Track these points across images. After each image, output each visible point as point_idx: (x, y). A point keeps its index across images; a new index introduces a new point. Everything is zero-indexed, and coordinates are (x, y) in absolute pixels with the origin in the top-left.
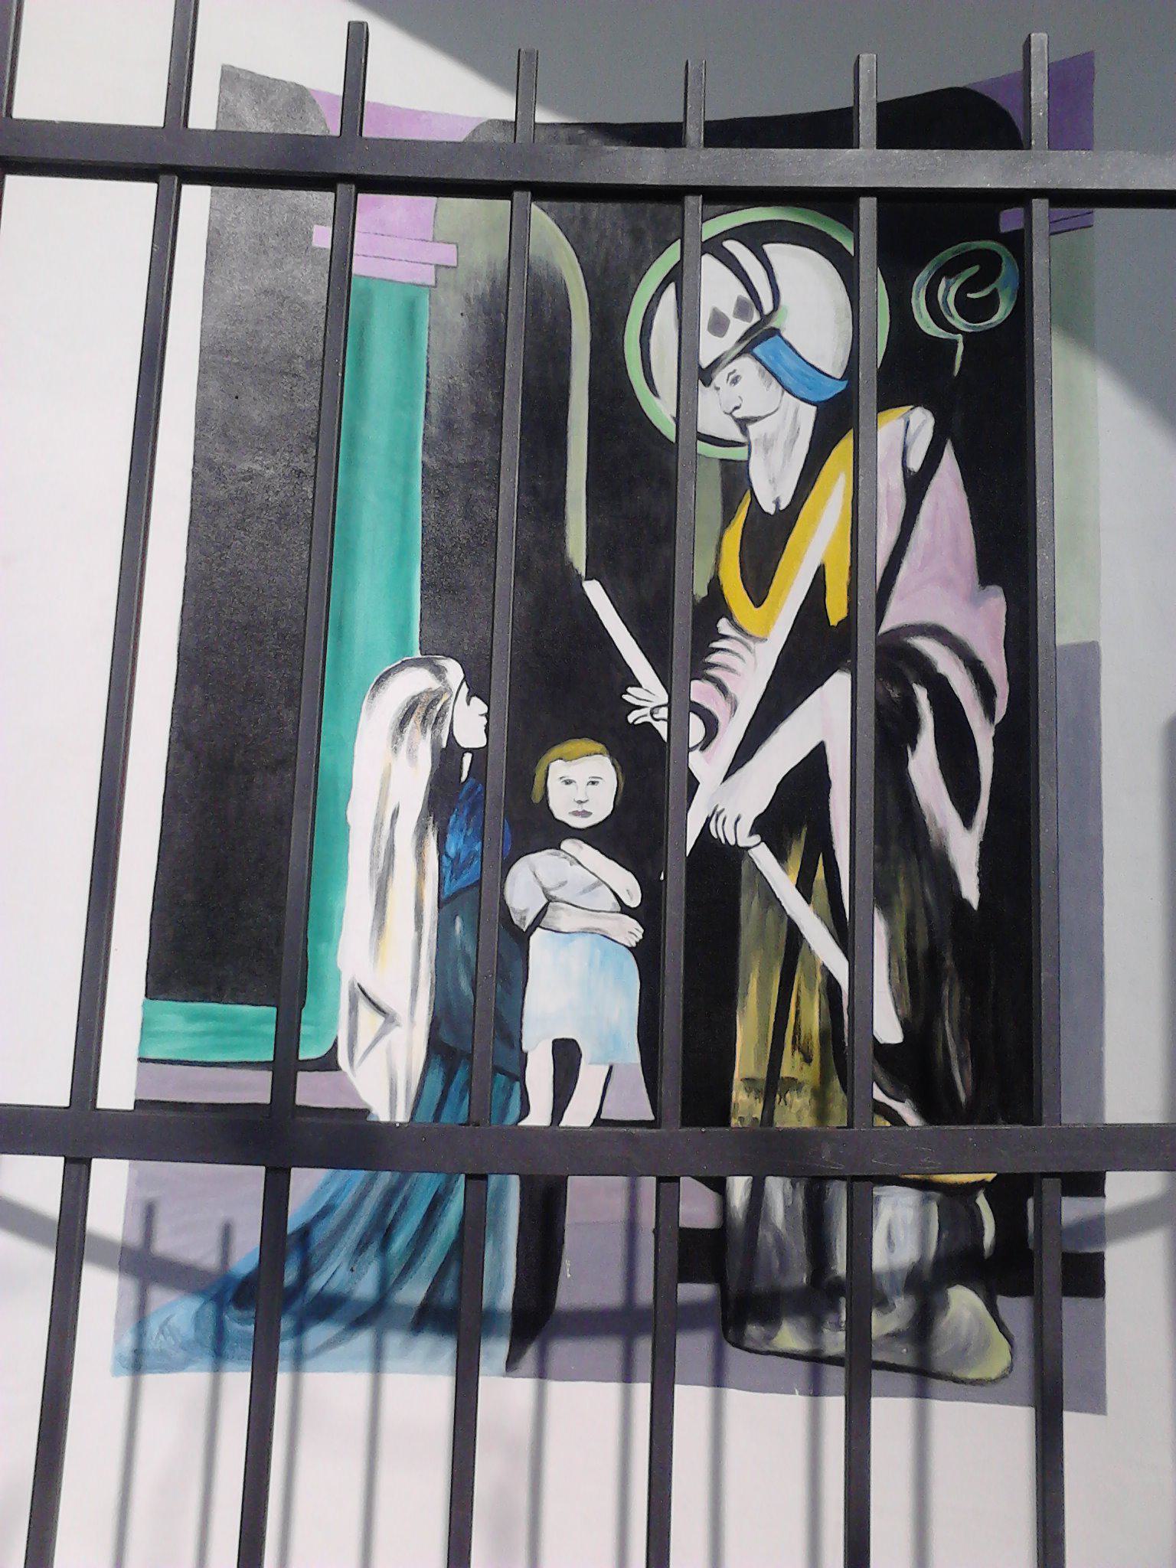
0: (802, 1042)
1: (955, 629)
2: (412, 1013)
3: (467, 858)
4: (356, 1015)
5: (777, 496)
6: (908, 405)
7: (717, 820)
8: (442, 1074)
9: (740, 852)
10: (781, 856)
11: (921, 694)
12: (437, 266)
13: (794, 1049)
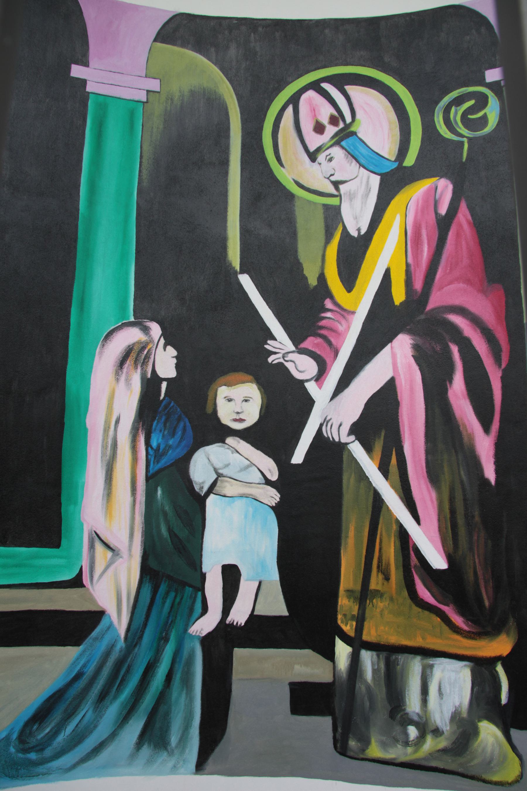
0: (383, 567)
1: (473, 309)
2: (130, 550)
3: (164, 449)
4: (94, 552)
5: (358, 227)
6: (436, 177)
7: (327, 426)
8: (150, 588)
9: (341, 447)
10: (368, 449)
11: (455, 350)
12: (148, 91)
13: (378, 571)
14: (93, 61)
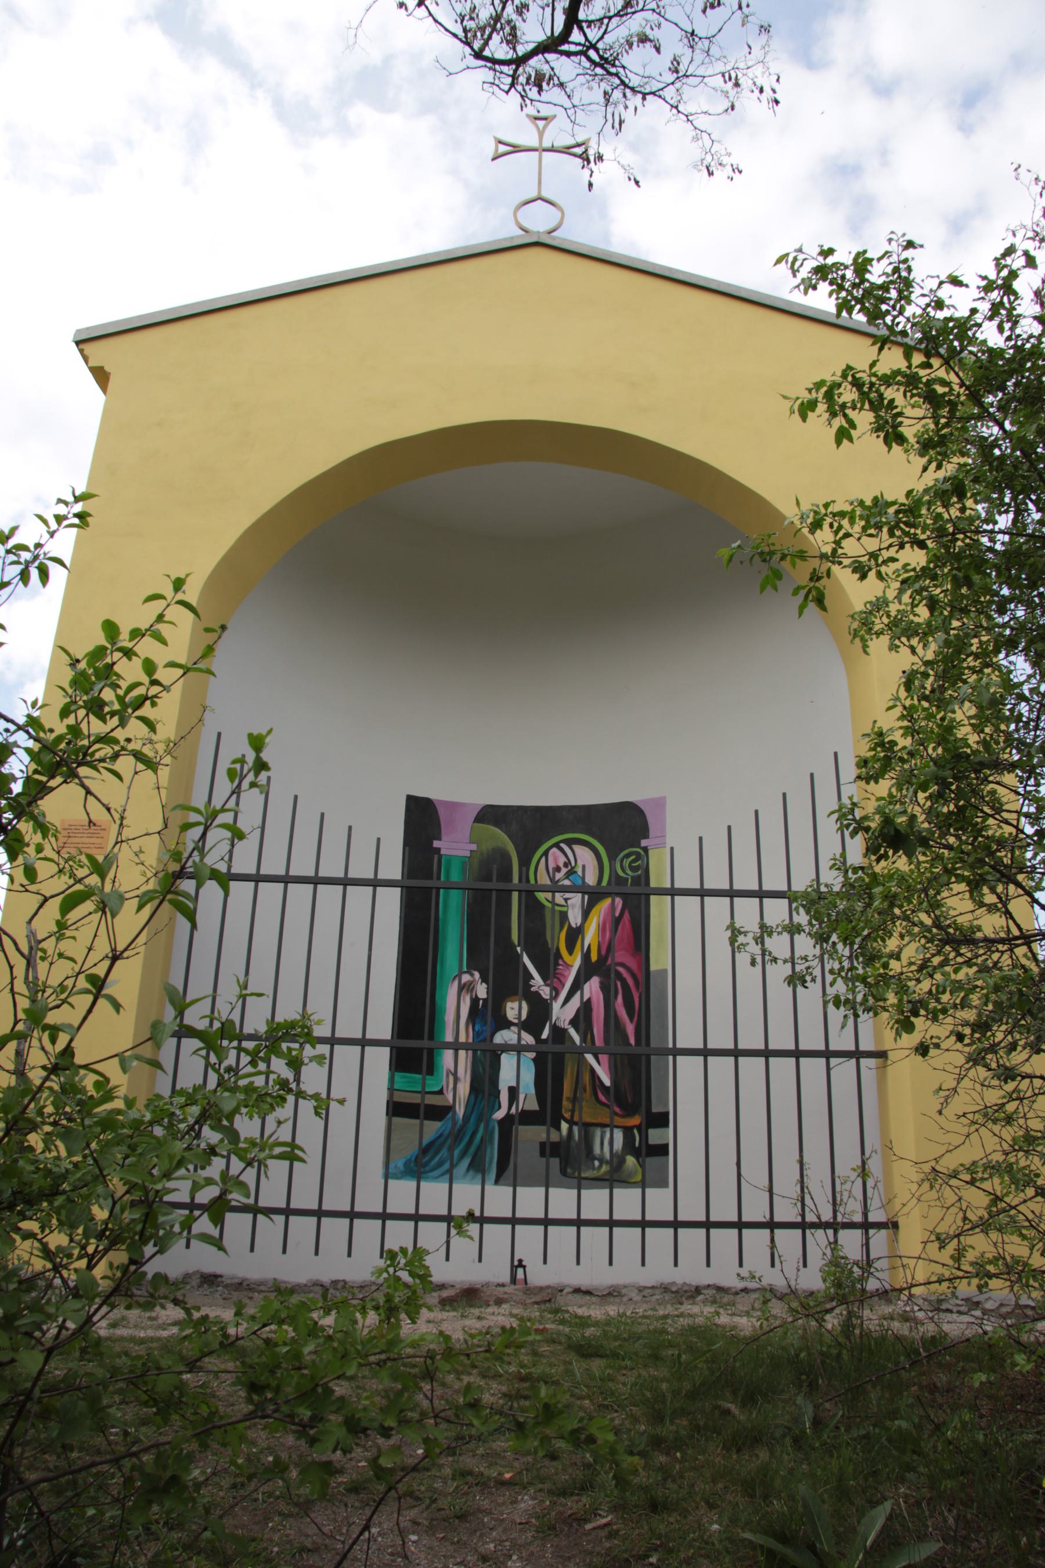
14: (444, 838)
